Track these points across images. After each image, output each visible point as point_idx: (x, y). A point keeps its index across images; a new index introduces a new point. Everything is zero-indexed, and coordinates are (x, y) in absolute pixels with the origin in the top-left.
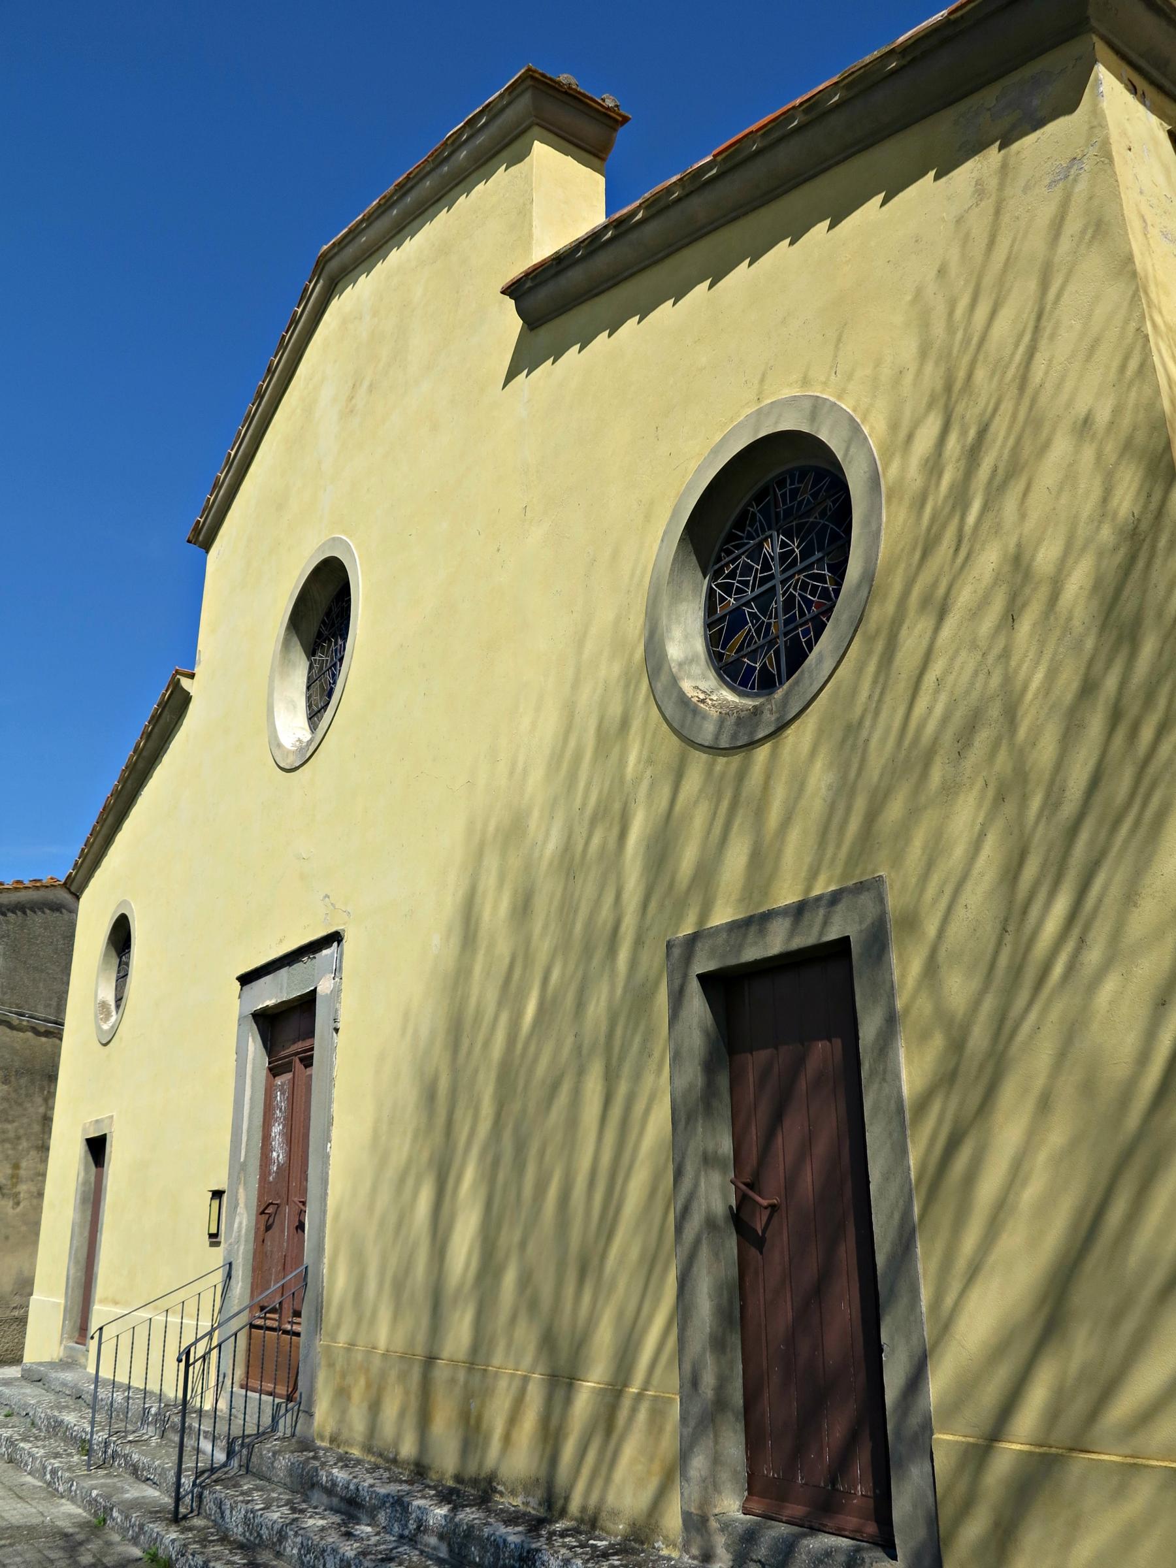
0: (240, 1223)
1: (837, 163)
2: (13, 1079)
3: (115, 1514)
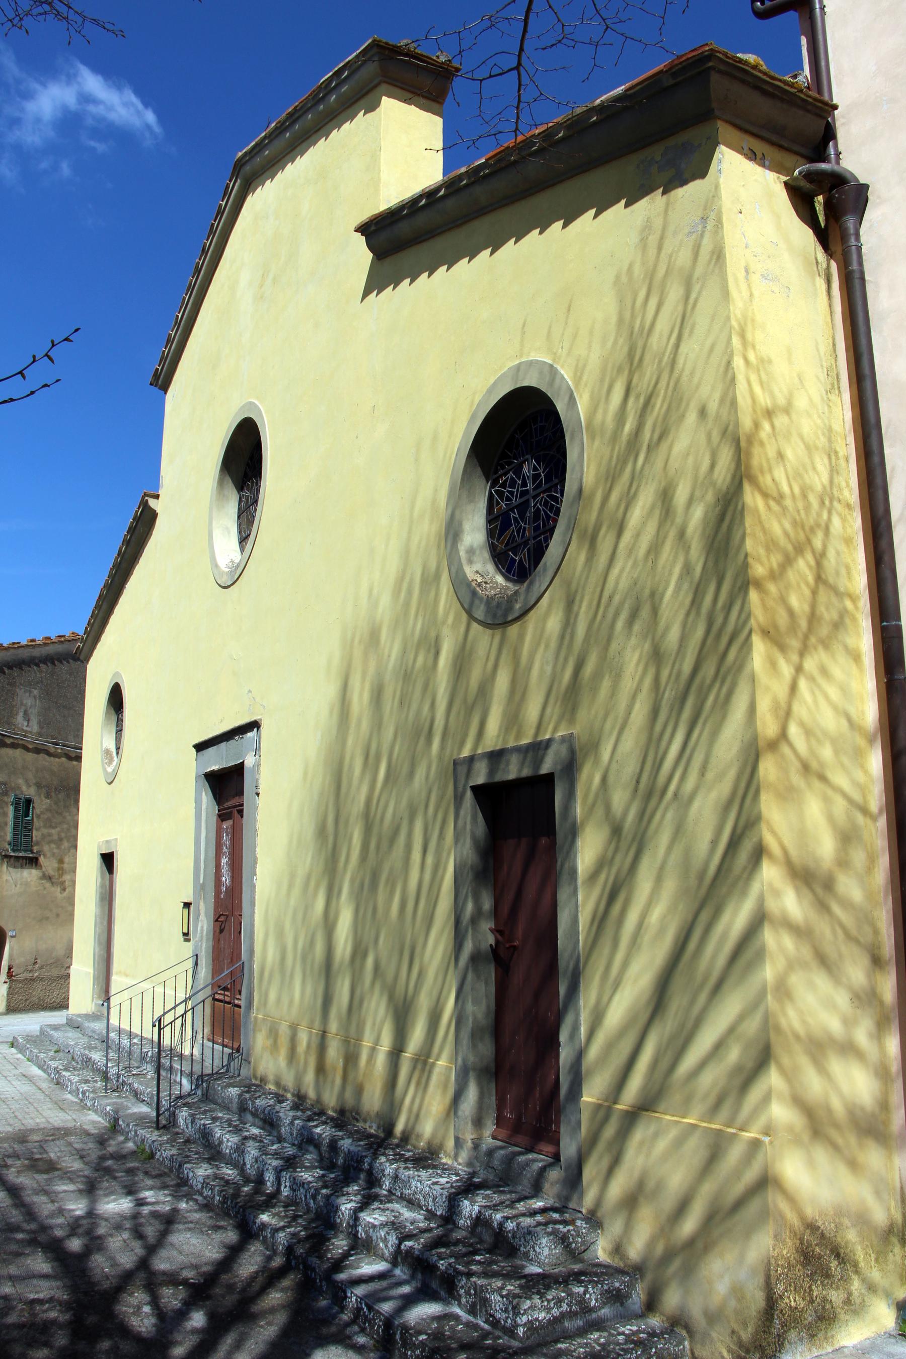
0: (202, 927)
1: (569, 178)
2: (53, 794)
3: (121, 1123)
